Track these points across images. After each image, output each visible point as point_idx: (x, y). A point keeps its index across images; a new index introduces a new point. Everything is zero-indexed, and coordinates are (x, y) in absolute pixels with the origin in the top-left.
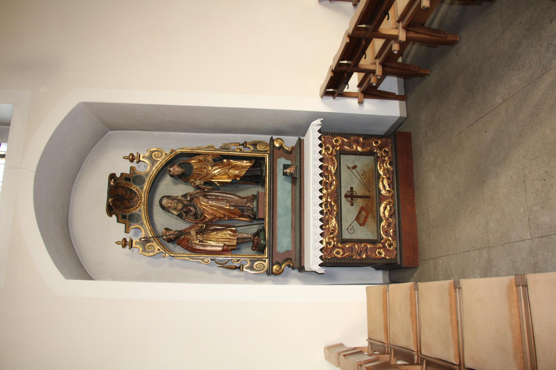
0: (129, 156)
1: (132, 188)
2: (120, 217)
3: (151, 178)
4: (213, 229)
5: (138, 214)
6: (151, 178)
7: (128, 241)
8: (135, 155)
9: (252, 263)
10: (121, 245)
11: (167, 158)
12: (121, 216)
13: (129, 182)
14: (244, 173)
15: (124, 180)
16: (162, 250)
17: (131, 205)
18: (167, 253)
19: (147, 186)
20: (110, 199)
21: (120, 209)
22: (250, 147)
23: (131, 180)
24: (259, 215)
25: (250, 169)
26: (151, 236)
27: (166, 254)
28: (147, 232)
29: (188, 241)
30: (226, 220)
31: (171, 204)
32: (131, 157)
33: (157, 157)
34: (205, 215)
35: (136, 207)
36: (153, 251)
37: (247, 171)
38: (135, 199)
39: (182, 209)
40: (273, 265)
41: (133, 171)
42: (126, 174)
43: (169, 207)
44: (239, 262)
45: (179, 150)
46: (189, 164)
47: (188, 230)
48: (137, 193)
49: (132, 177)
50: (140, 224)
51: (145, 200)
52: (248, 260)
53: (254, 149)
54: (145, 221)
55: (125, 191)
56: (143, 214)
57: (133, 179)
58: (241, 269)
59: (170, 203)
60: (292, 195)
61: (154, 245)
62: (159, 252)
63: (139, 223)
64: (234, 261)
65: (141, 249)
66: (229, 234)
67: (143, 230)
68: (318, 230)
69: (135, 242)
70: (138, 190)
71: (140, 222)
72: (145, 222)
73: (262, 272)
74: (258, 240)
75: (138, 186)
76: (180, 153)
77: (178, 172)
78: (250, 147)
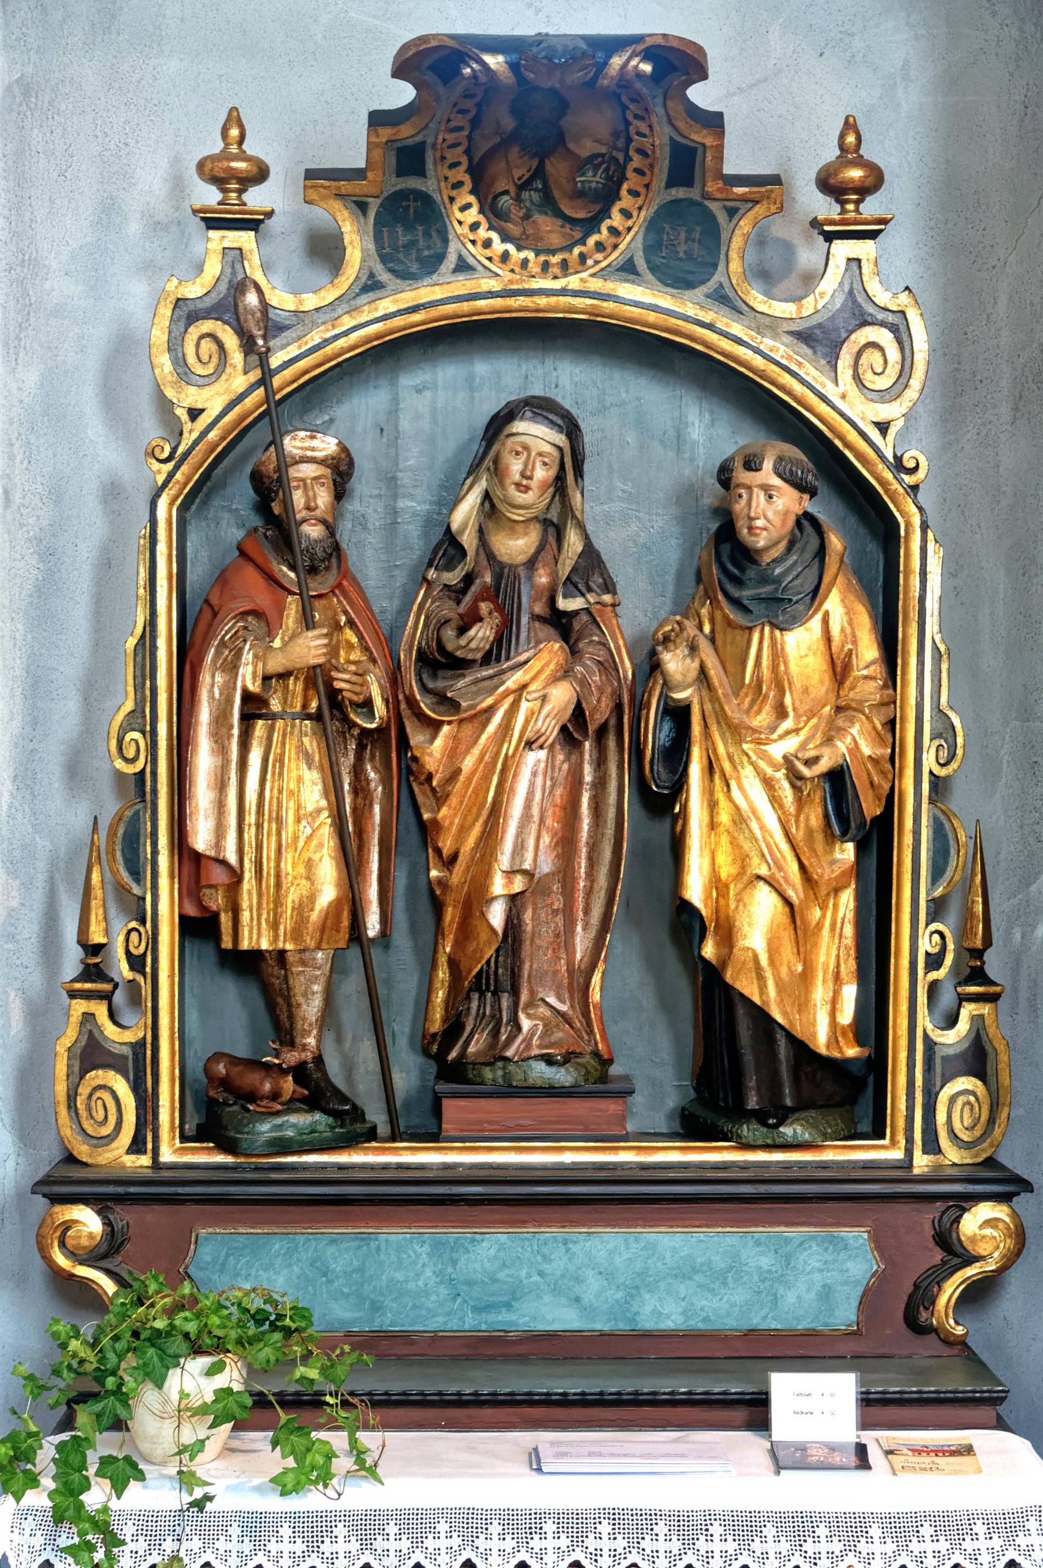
0: (860, 162)
1: (626, 201)
2: (406, 131)
3: (700, 331)
4: (368, 781)
5: (441, 257)
6: (700, 331)
7: (245, 197)
8: (872, 207)
9: (125, 1057)
10: (217, 147)
11: (853, 436)
12: (411, 142)
13: (665, 176)
14: (746, 992)
15: (671, 139)
16: (195, 435)
17: (505, 201)
18: (171, 476)
19: (637, 304)
20: (501, 58)
21: (460, 129)
22: (963, 1026)
23: (679, 193)
24: (462, 1102)
25: (782, 1042)
26: (275, 361)
27: (170, 466)
28: (315, 325)
29: (257, 614)
30: (428, 870)
31: (518, 485)
32: (855, 174)
33: (864, 360)
34: (449, 723)
35: (494, 236)
36: (183, 373)
37: (761, 1016)
38: (546, 224)
39: (491, 556)
40: (100, 1203)
41: (743, 198)
42: (720, 149)
43: (498, 472)
44: (124, 966)
45: (916, 520)
46: (816, 594)
47: (346, 613)
48: (591, 241)
49: (706, 196)
50: (372, 275)
51: (542, 301)
52: (141, 1035)
53: (944, 1058)
54: (392, 309)
55: (602, 155)
56: (438, 293)
57: (691, 202)
58: (78, 986)
59: (523, 475)
60: (603, 1334)
61: (224, 377)
62: (182, 414)
63: (379, 268)
64: (134, 936)
65: (194, 290)
66: (312, 898)
67: (330, 298)
68: (614, 1554)
69: (240, 249)
70: (615, 247)
71: (384, 276)
72: (387, 306)
73: (67, 1131)
74: (275, 1096)
75: (640, 238)
76: (897, 525)
77: (751, 519)
78: (963, 1026)
